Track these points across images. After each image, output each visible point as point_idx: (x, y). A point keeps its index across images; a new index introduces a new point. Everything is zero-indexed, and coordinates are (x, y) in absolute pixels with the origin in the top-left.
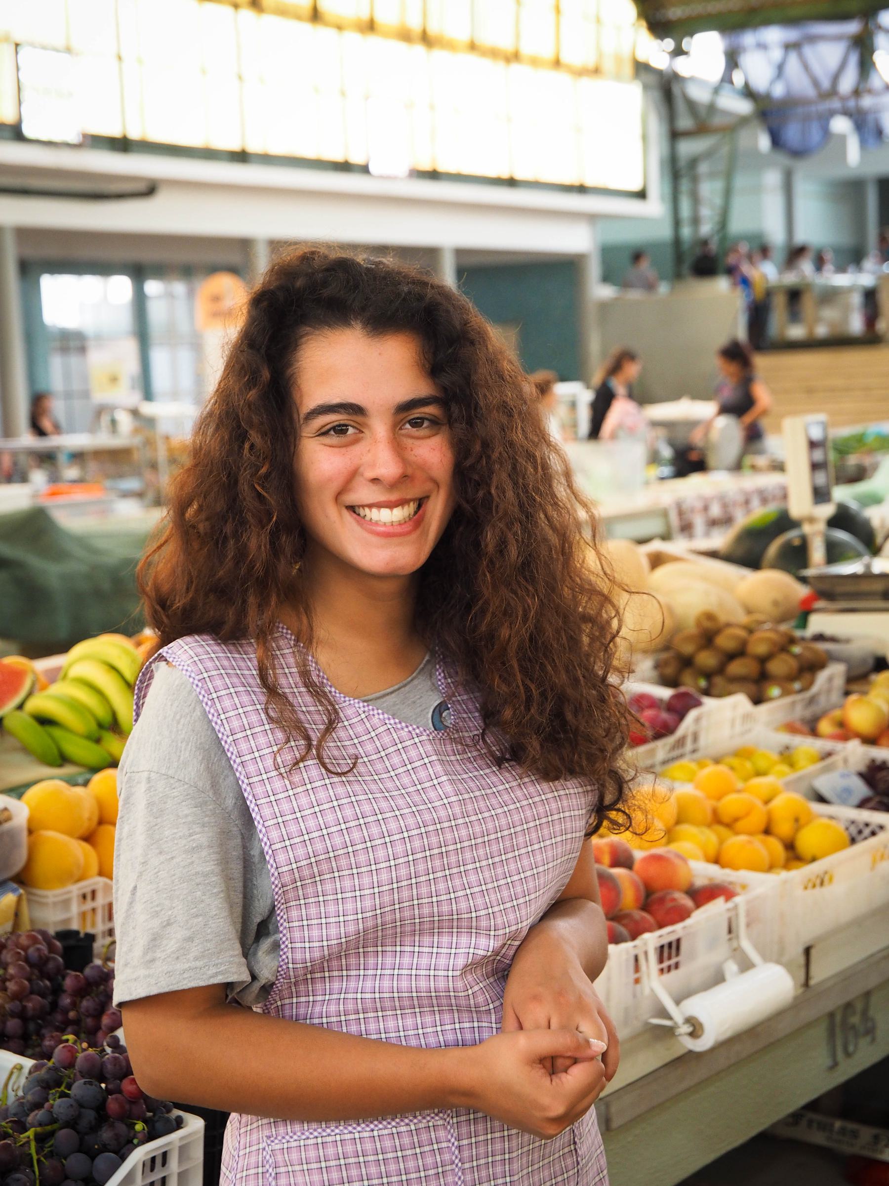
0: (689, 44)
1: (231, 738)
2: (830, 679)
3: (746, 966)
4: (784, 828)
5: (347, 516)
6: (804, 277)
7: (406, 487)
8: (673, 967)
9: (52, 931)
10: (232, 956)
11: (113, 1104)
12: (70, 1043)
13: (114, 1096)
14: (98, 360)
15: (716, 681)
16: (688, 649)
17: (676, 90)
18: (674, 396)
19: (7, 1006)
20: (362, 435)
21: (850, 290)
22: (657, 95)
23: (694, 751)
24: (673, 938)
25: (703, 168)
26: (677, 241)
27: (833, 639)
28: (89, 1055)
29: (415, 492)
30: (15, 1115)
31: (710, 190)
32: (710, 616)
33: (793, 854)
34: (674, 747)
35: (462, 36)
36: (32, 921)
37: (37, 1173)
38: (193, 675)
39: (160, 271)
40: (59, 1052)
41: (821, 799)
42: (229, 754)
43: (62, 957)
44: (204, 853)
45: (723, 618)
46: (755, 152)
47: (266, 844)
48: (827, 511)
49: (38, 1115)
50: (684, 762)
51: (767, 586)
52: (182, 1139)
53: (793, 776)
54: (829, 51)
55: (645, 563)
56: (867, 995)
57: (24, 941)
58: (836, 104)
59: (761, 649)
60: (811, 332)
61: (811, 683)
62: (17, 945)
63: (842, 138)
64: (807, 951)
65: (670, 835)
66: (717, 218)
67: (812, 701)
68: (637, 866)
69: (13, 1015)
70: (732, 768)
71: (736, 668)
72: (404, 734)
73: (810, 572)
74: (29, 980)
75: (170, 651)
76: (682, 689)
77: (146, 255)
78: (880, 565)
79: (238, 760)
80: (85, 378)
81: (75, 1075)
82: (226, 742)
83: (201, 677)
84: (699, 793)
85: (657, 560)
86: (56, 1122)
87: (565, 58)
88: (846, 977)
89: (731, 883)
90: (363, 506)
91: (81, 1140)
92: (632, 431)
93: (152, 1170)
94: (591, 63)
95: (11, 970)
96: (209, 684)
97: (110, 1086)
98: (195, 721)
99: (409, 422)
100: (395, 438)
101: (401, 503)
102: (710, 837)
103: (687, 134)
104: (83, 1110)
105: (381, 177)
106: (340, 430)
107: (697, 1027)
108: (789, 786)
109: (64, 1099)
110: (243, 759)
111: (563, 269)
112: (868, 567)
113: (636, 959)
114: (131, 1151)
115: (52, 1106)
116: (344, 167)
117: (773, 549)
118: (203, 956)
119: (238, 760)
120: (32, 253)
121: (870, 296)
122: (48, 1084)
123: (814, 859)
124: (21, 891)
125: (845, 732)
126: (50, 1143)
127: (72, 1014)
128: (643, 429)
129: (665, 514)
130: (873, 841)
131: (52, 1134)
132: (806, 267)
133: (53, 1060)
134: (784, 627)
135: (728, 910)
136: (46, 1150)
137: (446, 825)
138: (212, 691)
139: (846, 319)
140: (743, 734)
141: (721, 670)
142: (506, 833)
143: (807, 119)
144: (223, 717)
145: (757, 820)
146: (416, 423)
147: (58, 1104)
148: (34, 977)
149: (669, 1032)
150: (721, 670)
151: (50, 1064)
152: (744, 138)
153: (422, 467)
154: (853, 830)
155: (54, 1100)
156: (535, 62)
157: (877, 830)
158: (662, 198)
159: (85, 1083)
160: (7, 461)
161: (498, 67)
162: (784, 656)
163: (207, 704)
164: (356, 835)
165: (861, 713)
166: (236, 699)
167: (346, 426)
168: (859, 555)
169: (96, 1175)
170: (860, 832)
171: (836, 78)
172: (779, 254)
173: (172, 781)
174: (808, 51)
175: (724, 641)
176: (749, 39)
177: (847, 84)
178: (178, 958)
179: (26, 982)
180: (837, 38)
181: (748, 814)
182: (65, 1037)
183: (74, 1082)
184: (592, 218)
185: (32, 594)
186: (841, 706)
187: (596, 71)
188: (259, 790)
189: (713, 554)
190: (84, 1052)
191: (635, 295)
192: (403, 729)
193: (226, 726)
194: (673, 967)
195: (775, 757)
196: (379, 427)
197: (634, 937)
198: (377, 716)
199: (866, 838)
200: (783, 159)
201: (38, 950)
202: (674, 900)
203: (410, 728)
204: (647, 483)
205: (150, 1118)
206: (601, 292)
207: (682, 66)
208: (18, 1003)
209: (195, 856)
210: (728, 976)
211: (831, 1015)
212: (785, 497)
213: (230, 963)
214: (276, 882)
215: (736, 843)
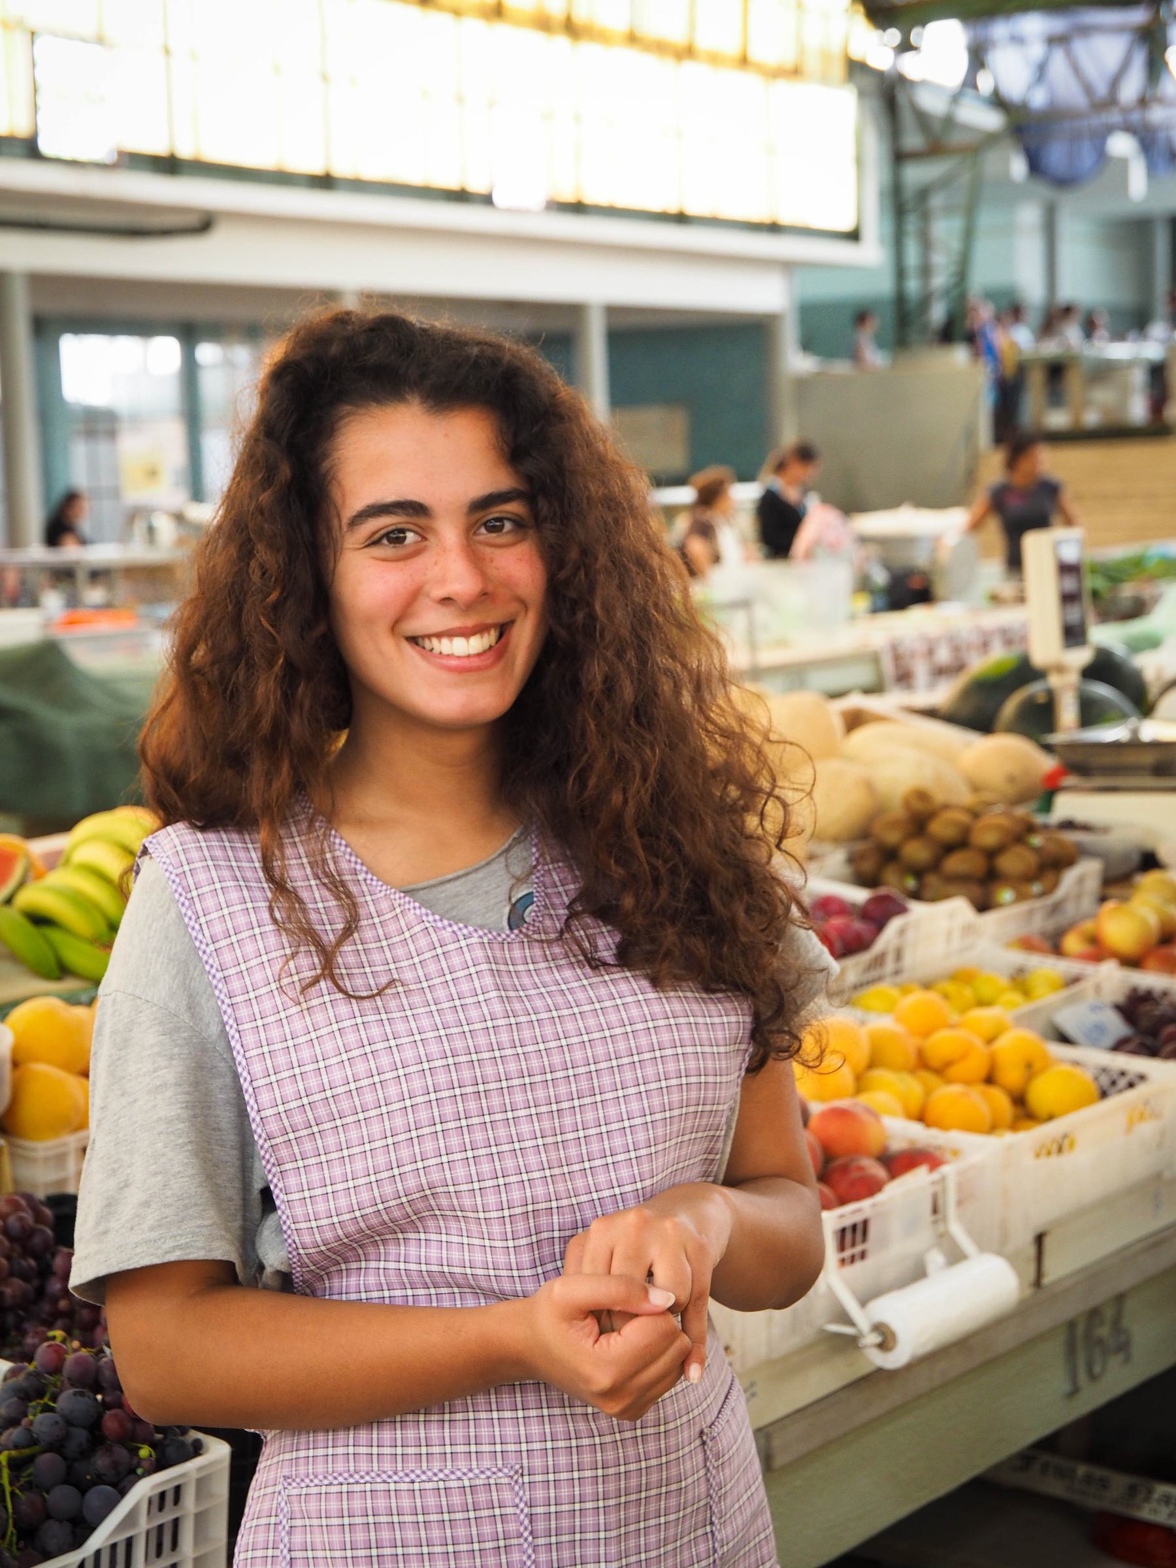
0: (920, 36)
1: (212, 947)
2: (1081, 880)
3: (956, 1257)
4: (1012, 1076)
5: (407, 648)
6: (1069, 347)
7: (486, 610)
9: (41, 1194)
11: (110, 1422)
12: (58, 1341)
13: (113, 1412)
14: (132, 448)
15: (927, 882)
16: (892, 837)
17: (902, 99)
18: (891, 502)
20: (426, 543)
21: (1130, 364)
22: (875, 104)
23: (897, 972)
24: (858, 1218)
25: (937, 201)
26: (900, 299)
27: (1086, 828)
28: (81, 1357)
29: (496, 615)
31: (946, 230)
32: (922, 795)
33: (1023, 1111)
36: (16, 1182)
39: (217, 331)
40: (42, 1351)
41: (1064, 1039)
43: (54, 1229)
45: (939, 797)
46: (1005, 181)
47: (245, 1079)
48: (1081, 657)
51: (1001, 755)
52: (200, 1469)
53: (1026, 1007)
54: (1106, 48)
55: (838, 724)
56: (1120, 1298)
58: (1115, 117)
59: (988, 839)
60: (1077, 420)
61: (1055, 885)
63: (1123, 163)
64: (1039, 1239)
65: (860, 1084)
66: (953, 268)
67: (1056, 908)
70: (946, 996)
71: (956, 863)
72: (447, 934)
73: (1057, 738)
74: (9, 1258)
75: (154, 841)
78: (1152, 730)
80: (115, 470)
81: (62, 1382)
82: (204, 952)
83: (180, 870)
84: (899, 1029)
85: (854, 721)
86: (36, 1444)
87: (755, 55)
88: (1092, 1274)
89: (939, 1148)
90: (429, 636)
91: (69, 1468)
92: (833, 549)
93: (161, 1508)
97: (108, 1399)
99: (485, 524)
100: (469, 546)
101: (479, 630)
102: (913, 1087)
103: (916, 156)
104: (72, 1429)
105: (510, 211)
106: (395, 537)
108: (1022, 1020)
110: (226, 973)
111: (748, 334)
112: (1135, 732)
114: (132, 1484)
115: (31, 1423)
116: (460, 196)
117: (1010, 707)
119: (219, 975)
120: (52, 306)
121: (1157, 372)
123: (1050, 1118)
125: (1098, 950)
126: (29, 1472)
129: (875, 659)
130: (1130, 1095)
131: (30, 1459)
132: (1072, 334)
133: (35, 1363)
134: (1021, 811)
135: (933, 1183)
136: (23, 1480)
139: (1123, 404)
141: (935, 866)
143: (1076, 138)
145: (975, 1065)
146: (494, 527)
147: (39, 1421)
148: (15, 1255)
149: (849, 1344)
150: (935, 866)
151: (31, 1368)
152: (991, 162)
153: (507, 583)
154: (1105, 1080)
155: (34, 1415)
156: (715, 59)
157: (1136, 1081)
158: (882, 240)
159: (75, 1394)
160: (11, 579)
161: (665, 66)
162: (1019, 850)
163: (183, 904)
164: (361, 1068)
165: (1124, 924)
167: (403, 531)
168: (1123, 717)
170: (1114, 1083)
171: (1115, 82)
172: (1034, 316)
173: (139, 1002)
174: (1080, 47)
175: (940, 828)
176: (1000, 30)
177: (1130, 89)
178: (132, 1228)
179: (4, 1262)
180: (1118, 30)
181: (964, 1056)
182: (51, 1334)
183: (61, 1391)
184: (788, 267)
185: (39, 754)
186: (1094, 916)
187: (796, 72)
188: (243, 1012)
189: (931, 713)
190: (76, 1352)
191: (841, 368)
192: (444, 928)
195: (1004, 981)
196: (449, 532)
198: (412, 911)
199: (1120, 1091)
200: (1043, 191)
201: (21, 1219)
202: (861, 1168)
203: (455, 928)
204: (853, 617)
205: (160, 1441)
206: (796, 362)
207: (911, 66)
209: (159, 1097)
211: (1071, 1325)
212: (1024, 639)
215: (947, 1094)
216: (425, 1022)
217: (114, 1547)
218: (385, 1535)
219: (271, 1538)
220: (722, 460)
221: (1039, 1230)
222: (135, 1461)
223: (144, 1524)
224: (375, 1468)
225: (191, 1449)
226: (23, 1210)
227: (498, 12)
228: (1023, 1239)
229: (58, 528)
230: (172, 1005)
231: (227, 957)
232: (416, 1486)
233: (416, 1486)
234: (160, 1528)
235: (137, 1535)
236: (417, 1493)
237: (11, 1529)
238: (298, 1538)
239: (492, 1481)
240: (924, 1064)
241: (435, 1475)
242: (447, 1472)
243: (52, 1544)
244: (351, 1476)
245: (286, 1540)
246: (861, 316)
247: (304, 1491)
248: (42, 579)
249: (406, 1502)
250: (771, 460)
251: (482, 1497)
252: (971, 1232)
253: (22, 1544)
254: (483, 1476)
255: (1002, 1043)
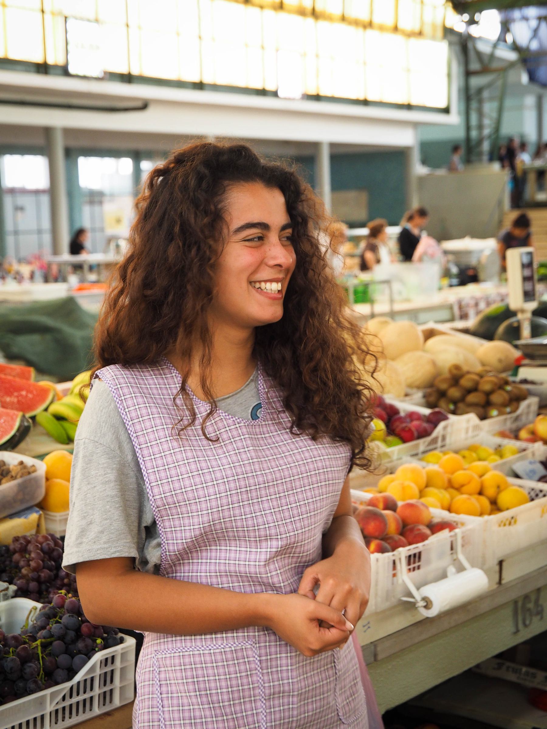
1: (131, 422)
2: (529, 406)
3: (461, 569)
4: (490, 491)
8: (416, 568)
10: (125, 543)
11: (84, 628)
12: (63, 594)
13: (85, 624)
14: (109, 209)
17: (470, 45)
18: (461, 236)
19: (30, 575)
22: (458, 48)
23: (443, 446)
24: (416, 551)
25: (486, 94)
26: (468, 139)
27: (533, 383)
28: (72, 601)
30: (31, 633)
31: (490, 108)
32: (457, 367)
33: (495, 506)
34: (430, 444)
35: (337, 12)
36: (47, 530)
37: (41, 664)
38: (112, 386)
40: (56, 598)
41: (517, 476)
42: (129, 432)
44: (112, 484)
45: (465, 368)
48: (533, 305)
49: (44, 632)
50: (436, 452)
51: (494, 350)
52: (122, 649)
53: (499, 461)
57: (40, 539)
59: (486, 387)
61: (517, 408)
62: (37, 541)
64: (501, 563)
65: (422, 494)
67: (517, 419)
68: (398, 510)
69: (33, 580)
70: (464, 457)
71: (472, 398)
72: (230, 422)
74: (43, 561)
75: (101, 373)
76: (437, 410)
77: (141, 146)
79: (135, 435)
81: (64, 612)
82: (128, 425)
83: (116, 387)
84: (440, 470)
87: (401, 26)
88: (525, 580)
91: (67, 648)
93: (106, 665)
94: (417, 29)
95: (33, 555)
96: (121, 391)
98: (111, 411)
102: (446, 496)
104: (68, 631)
107: (429, 603)
108: (496, 468)
109: (58, 624)
110: (138, 434)
111: (397, 156)
113: (394, 562)
114: (93, 654)
116: (263, 93)
117: (501, 329)
118: (108, 542)
119: (135, 435)
120: (73, 143)
122: (50, 616)
124: (41, 512)
125: (534, 437)
126: (50, 649)
127: (66, 581)
128: (439, 255)
129: (451, 307)
131: (51, 643)
134: (504, 375)
135: (451, 536)
136: (47, 652)
137: (250, 475)
138: (122, 395)
140: (473, 437)
141: (462, 399)
142: (288, 479)
144: (127, 410)
145: (474, 486)
147: (54, 627)
148: (46, 559)
149: (411, 606)
150: (462, 399)
151: (52, 605)
152: (512, 76)
154: (533, 494)
155: (52, 625)
156: (382, 28)
158: (459, 113)
159: (69, 616)
162: (501, 392)
163: (118, 403)
166: (135, 400)
169: (74, 667)
170: (537, 495)
172: (531, 148)
173: (97, 444)
175: (465, 382)
176: (517, 14)
178: (95, 542)
179: (41, 562)
181: (469, 483)
182: (60, 591)
184: (416, 125)
186: (533, 422)
187: (420, 34)
188: (145, 452)
189: (466, 331)
190: (70, 599)
191: (441, 172)
192: (230, 419)
193: (128, 415)
194: (416, 568)
195: (491, 451)
197: (393, 550)
199: (540, 498)
200: (537, 89)
201: (48, 544)
202: (419, 530)
204: (440, 289)
205: (106, 637)
206: (419, 169)
207: (474, 31)
208: (36, 573)
210: (449, 574)
211: (516, 602)
213: (124, 546)
214: (153, 504)
215: (461, 499)
216: (224, 461)
217: (85, 681)
218: (200, 672)
219: (151, 677)
220: (383, 217)
221: (501, 559)
222: (95, 645)
223: (98, 671)
224: (194, 645)
225: (119, 641)
226: (48, 540)
227: (281, 7)
228: (493, 563)
229: (76, 247)
230: (112, 446)
231: (138, 427)
232: (212, 651)
233: (212, 651)
234: (106, 673)
235: (95, 676)
236: (213, 654)
237: (42, 672)
238: (163, 676)
239: (244, 647)
240: (452, 486)
241: (220, 646)
242: (224, 644)
243: (59, 679)
244: (184, 649)
245: (158, 677)
246: (456, 148)
247: (164, 656)
248: (69, 269)
249: (208, 658)
250: (407, 215)
251: (240, 654)
252: (468, 559)
253: (46, 678)
254: (240, 645)
255: (486, 477)
